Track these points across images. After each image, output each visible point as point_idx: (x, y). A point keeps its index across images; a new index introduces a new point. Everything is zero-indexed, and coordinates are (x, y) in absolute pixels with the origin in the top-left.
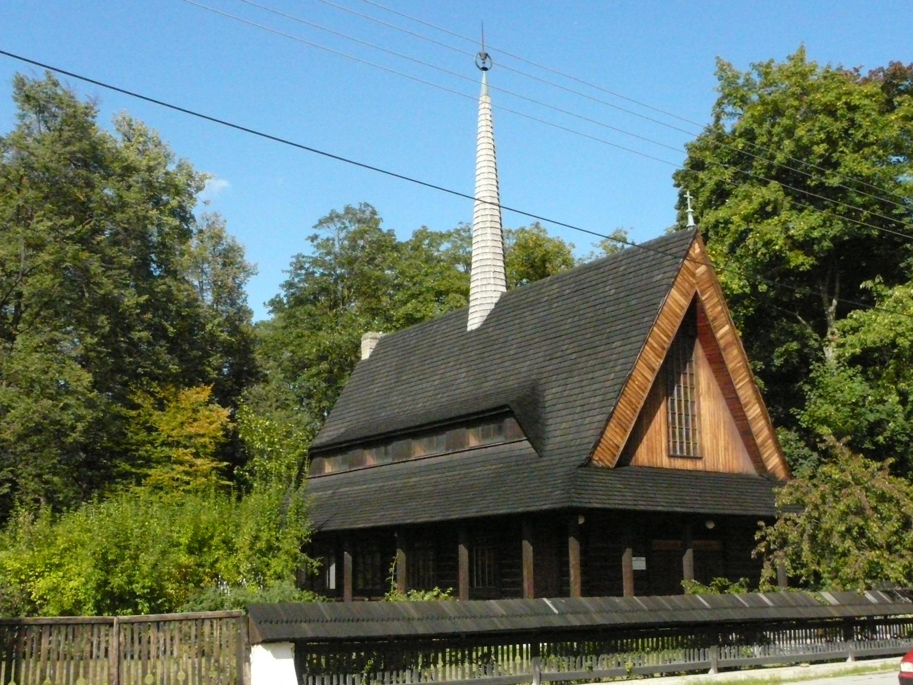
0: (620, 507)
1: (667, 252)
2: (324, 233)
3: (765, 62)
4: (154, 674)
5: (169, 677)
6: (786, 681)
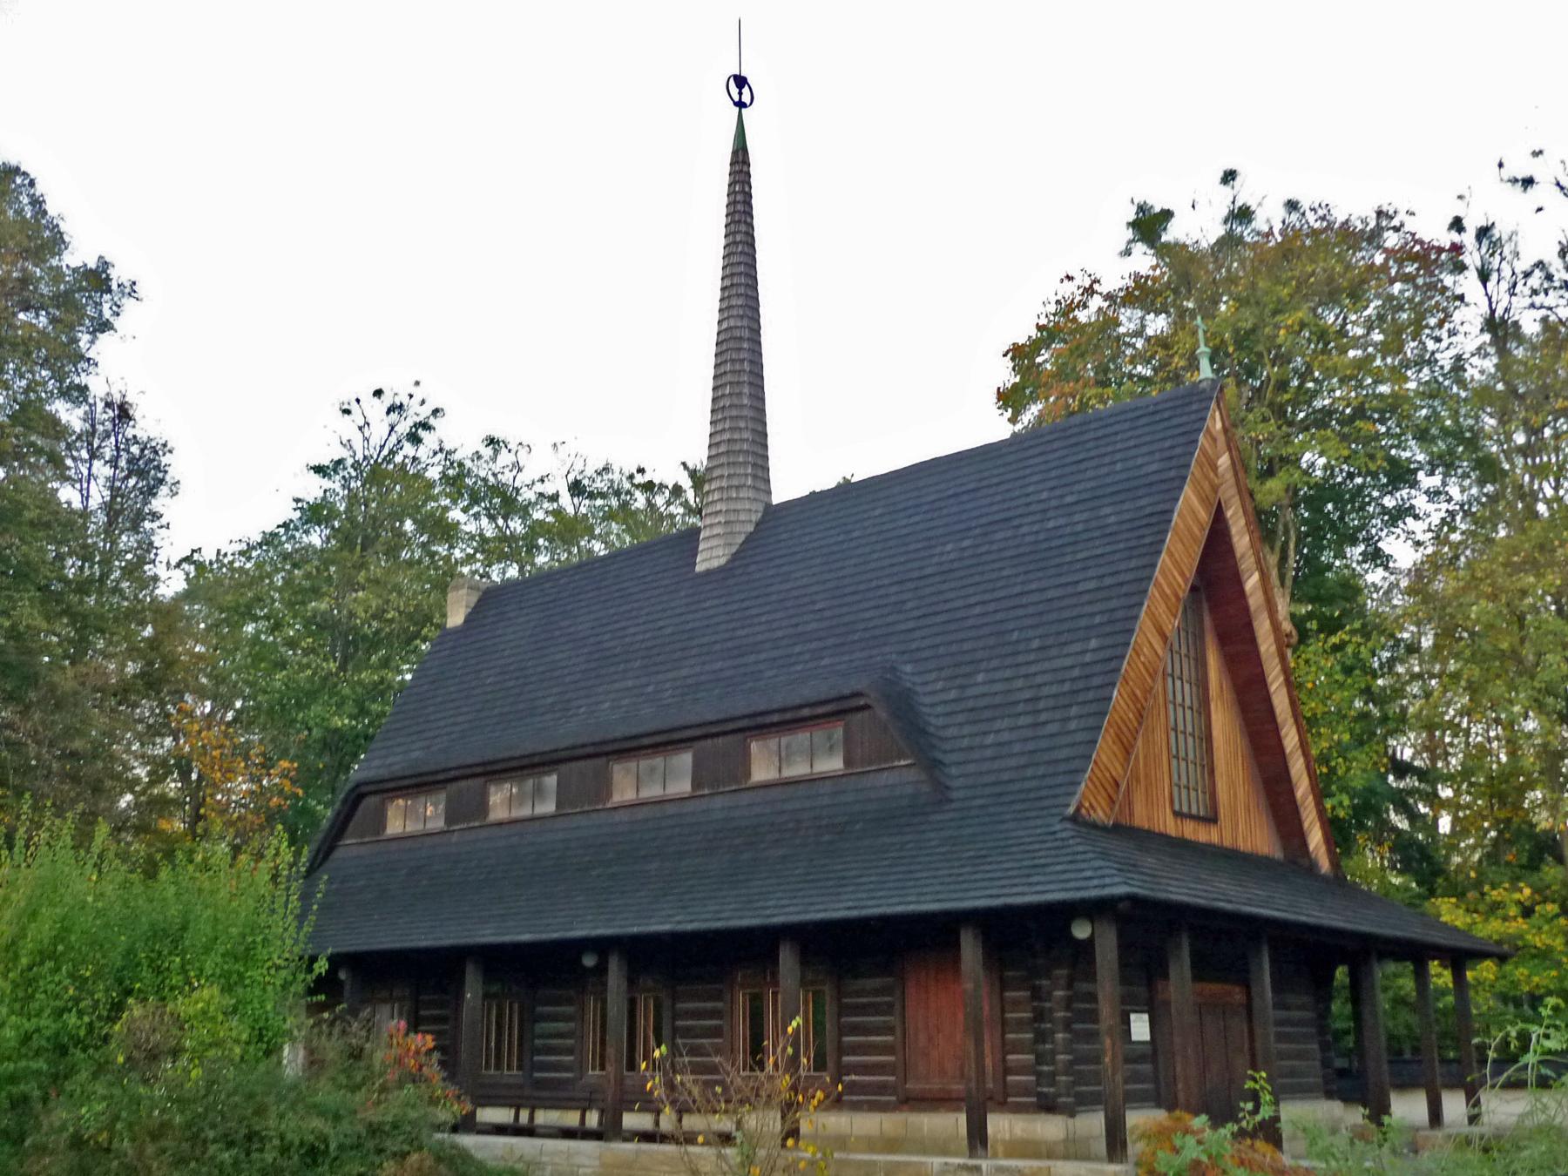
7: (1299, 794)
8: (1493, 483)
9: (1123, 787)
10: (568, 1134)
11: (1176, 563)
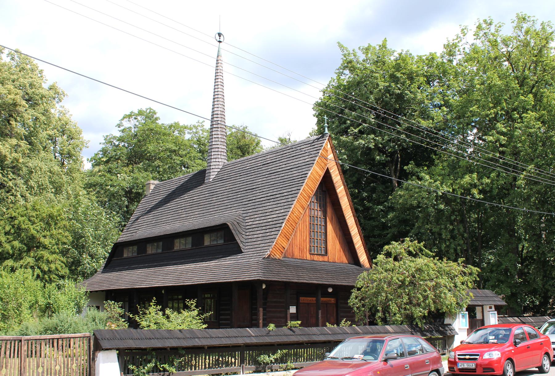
0: (285, 280)
1: (311, 146)
2: (126, 124)
3: (366, 46)
4: (43, 367)
5: (51, 369)
6: (346, 374)
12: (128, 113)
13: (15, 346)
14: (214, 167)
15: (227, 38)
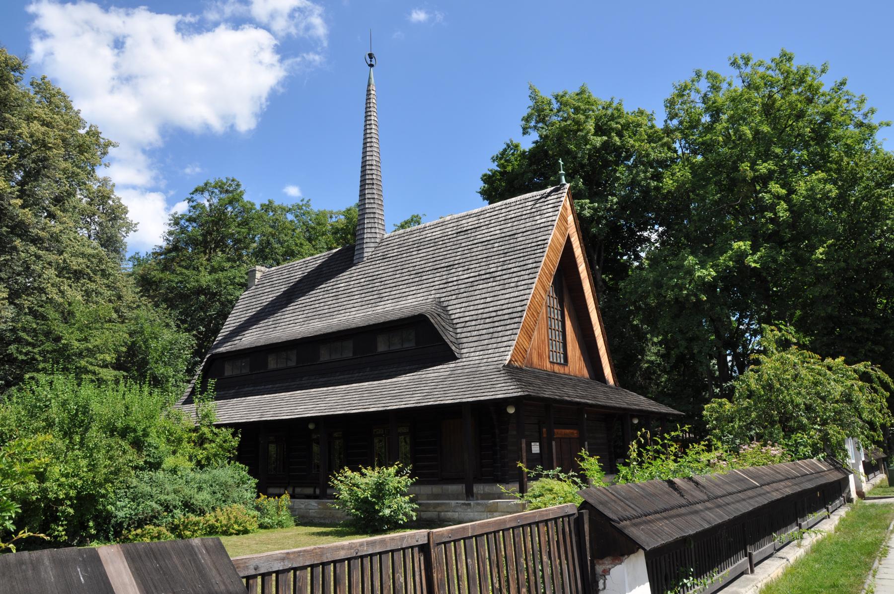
2: (204, 201)
7: (601, 353)
8: (649, 265)
9: (529, 351)
10: (308, 497)
11: (551, 261)
12: (202, 184)
13: (421, 575)
14: (368, 240)
15: (378, 61)
